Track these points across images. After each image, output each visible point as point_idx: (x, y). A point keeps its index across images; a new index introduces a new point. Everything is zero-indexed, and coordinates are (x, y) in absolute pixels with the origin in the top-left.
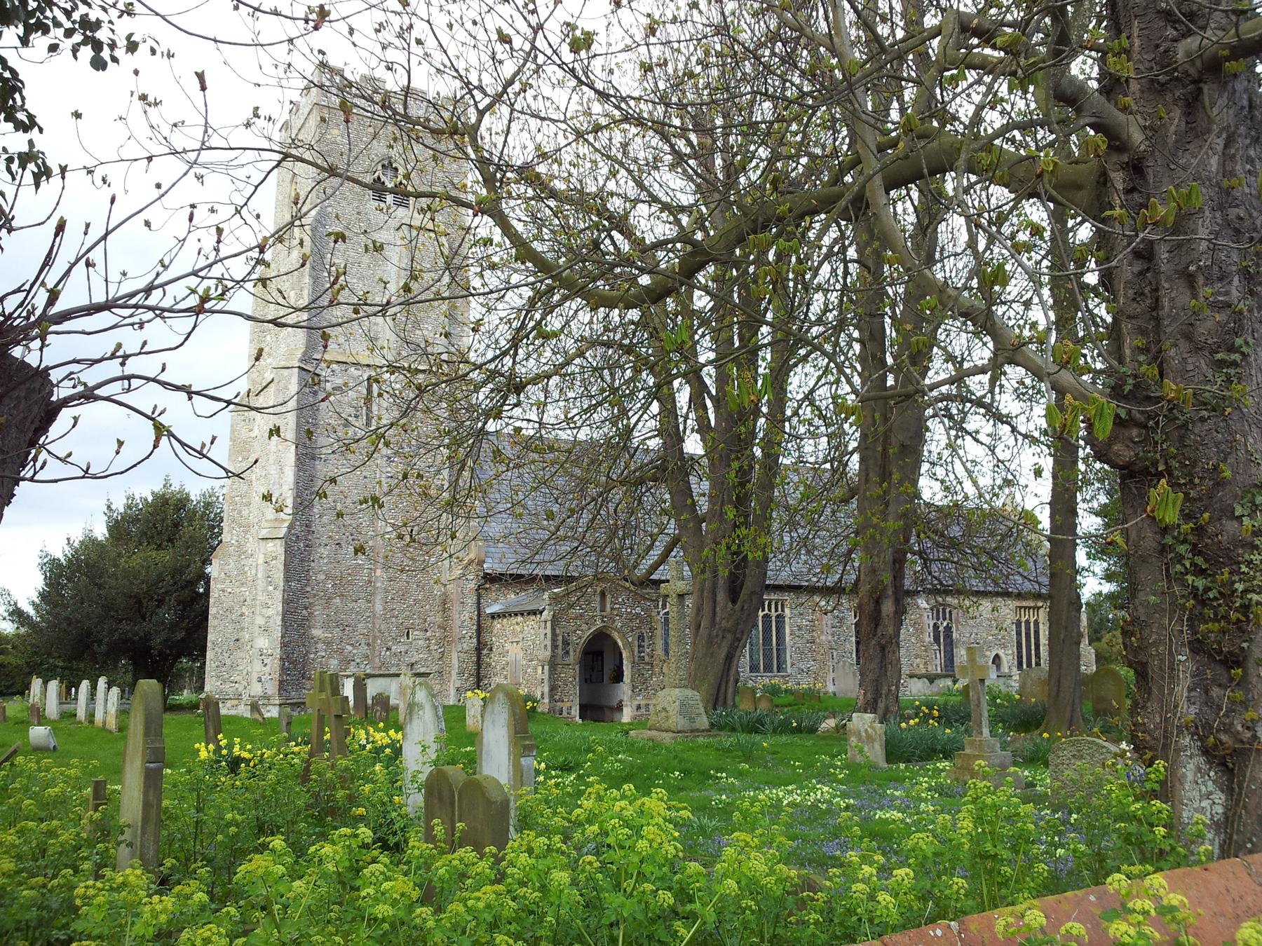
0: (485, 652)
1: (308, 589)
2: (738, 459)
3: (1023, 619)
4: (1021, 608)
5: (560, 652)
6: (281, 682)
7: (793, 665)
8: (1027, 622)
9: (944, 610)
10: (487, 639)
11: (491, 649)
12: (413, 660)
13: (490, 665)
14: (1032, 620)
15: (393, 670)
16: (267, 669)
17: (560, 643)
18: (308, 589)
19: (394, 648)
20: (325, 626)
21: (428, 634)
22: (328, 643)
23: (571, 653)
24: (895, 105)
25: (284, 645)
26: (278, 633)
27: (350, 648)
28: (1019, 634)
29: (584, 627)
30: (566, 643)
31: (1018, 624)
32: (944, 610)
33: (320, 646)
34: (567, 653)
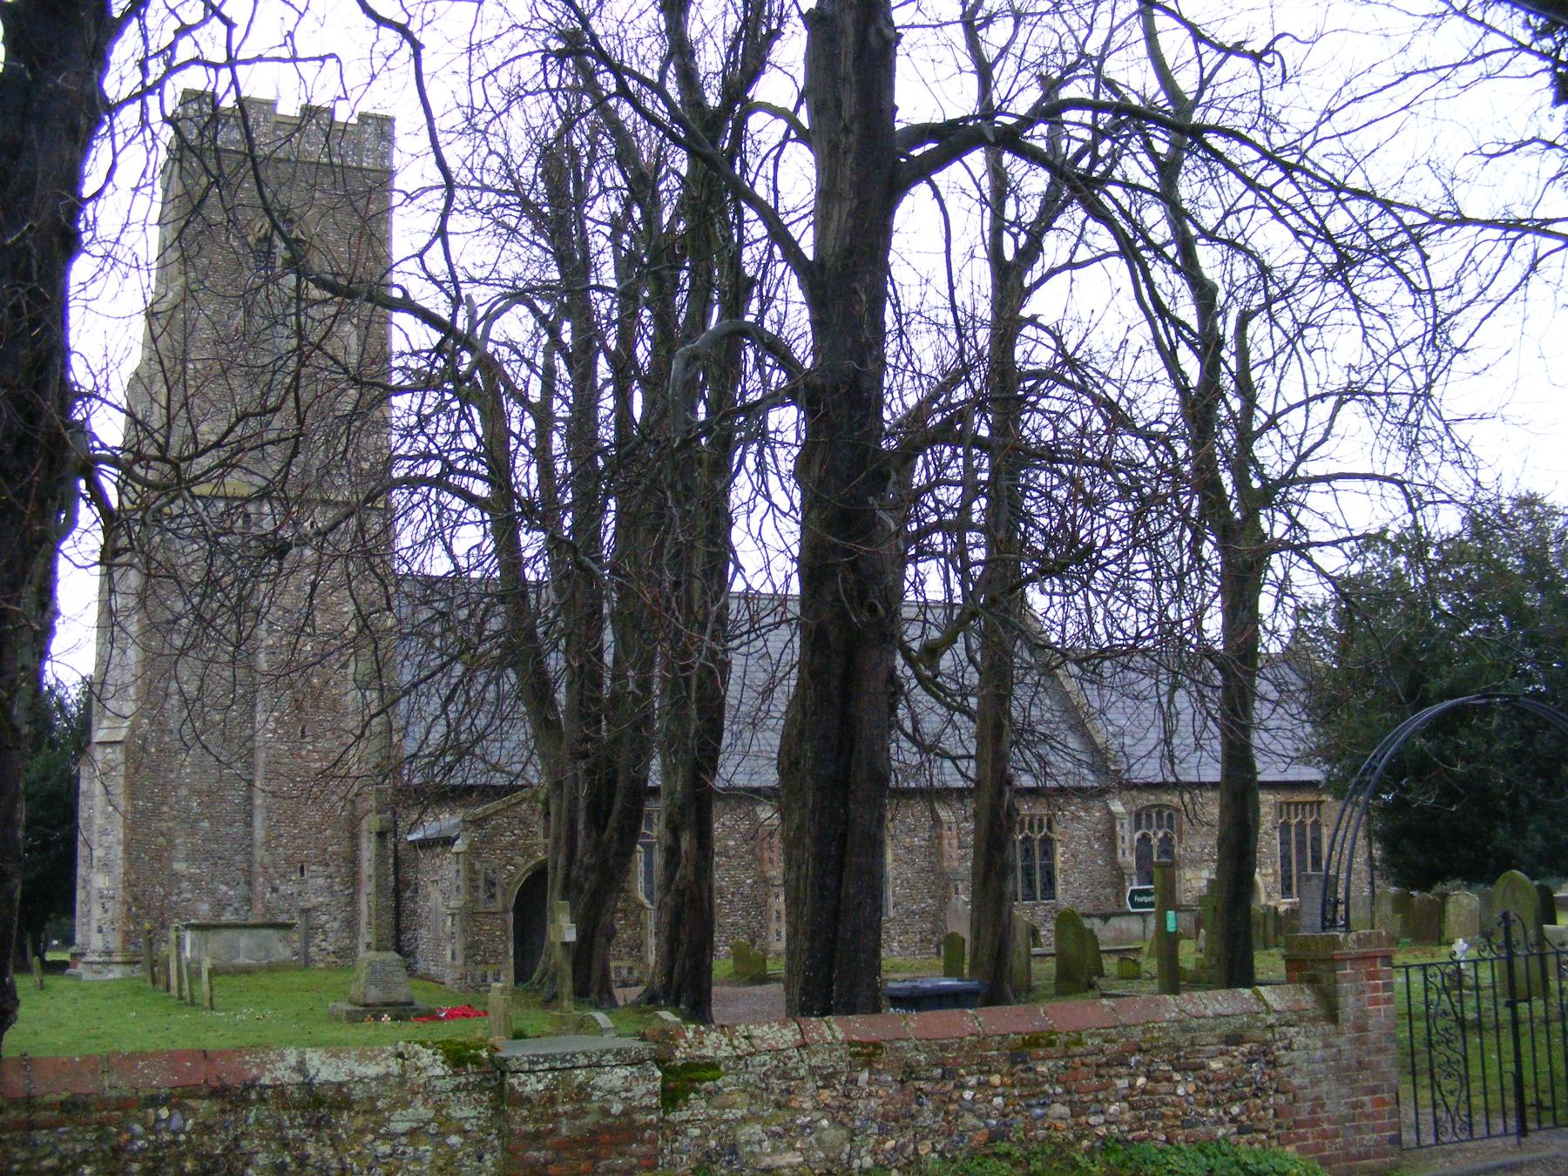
0: (408, 894)
1: (165, 809)
2: (211, 582)
3: (1294, 821)
4: (1289, 804)
5: (482, 895)
6: (127, 933)
7: (895, 906)
8: (1301, 824)
9: (1159, 814)
10: (411, 876)
11: (416, 891)
12: (309, 905)
13: (414, 912)
14: (1309, 821)
15: (282, 918)
16: (109, 915)
17: (481, 883)
18: (165, 809)
19: (282, 888)
20: (190, 858)
21: (331, 869)
22: (195, 881)
23: (499, 898)
24: (750, 214)
25: (129, 885)
26: (119, 870)
27: (224, 888)
28: (1285, 843)
29: (519, 860)
30: (491, 883)
31: (1285, 827)
32: (1159, 814)
33: (185, 884)
34: (492, 896)
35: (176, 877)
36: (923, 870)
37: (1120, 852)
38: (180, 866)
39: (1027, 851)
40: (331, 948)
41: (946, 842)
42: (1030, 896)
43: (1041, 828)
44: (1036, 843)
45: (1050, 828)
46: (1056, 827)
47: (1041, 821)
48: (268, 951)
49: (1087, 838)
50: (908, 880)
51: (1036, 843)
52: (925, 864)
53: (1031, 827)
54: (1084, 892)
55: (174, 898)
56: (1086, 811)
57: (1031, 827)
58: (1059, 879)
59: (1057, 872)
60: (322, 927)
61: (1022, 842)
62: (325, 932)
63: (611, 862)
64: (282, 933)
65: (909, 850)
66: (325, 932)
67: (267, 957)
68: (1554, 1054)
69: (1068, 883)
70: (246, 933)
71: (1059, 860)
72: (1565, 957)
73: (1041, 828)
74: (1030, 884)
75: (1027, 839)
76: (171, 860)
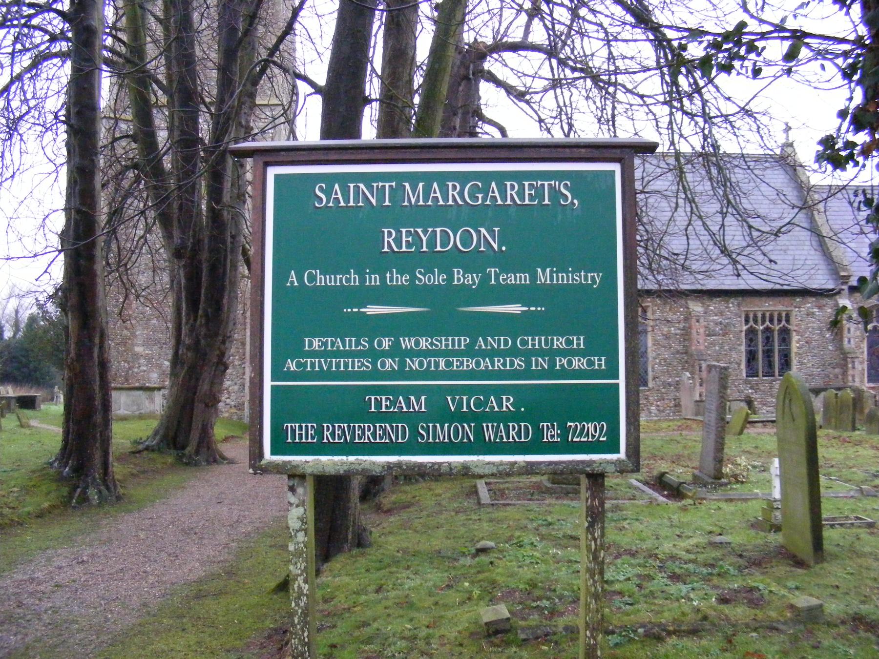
7: (654, 379)
20: (146, 344)
22: (149, 359)
33: (142, 361)
35: (137, 356)
36: (678, 352)
37: (846, 341)
38: (139, 349)
39: (768, 338)
40: (233, 403)
41: (694, 332)
42: (769, 373)
43: (780, 321)
44: (776, 333)
45: (788, 321)
46: (793, 319)
47: (780, 315)
48: (138, 405)
49: (820, 329)
50: (665, 360)
51: (776, 333)
52: (680, 348)
53: (771, 321)
54: (816, 371)
55: (136, 370)
56: (820, 307)
57: (771, 321)
58: (794, 361)
59: (793, 355)
60: (227, 389)
61: (764, 331)
62: (229, 393)
63: (203, 342)
64: (148, 393)
65: (667, 337)
66: (229, 393)
67: (139, 409)
68: (567, 150)
69: (801, 363)
70: (124, 393)
71: (794, 346)
72: (3, 136)
73: (780, 321)
74: (770, 365)
75: (767, 329)
76: (133, 345)
